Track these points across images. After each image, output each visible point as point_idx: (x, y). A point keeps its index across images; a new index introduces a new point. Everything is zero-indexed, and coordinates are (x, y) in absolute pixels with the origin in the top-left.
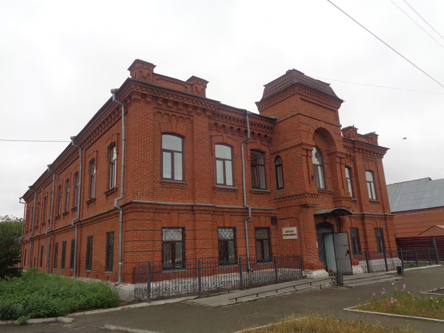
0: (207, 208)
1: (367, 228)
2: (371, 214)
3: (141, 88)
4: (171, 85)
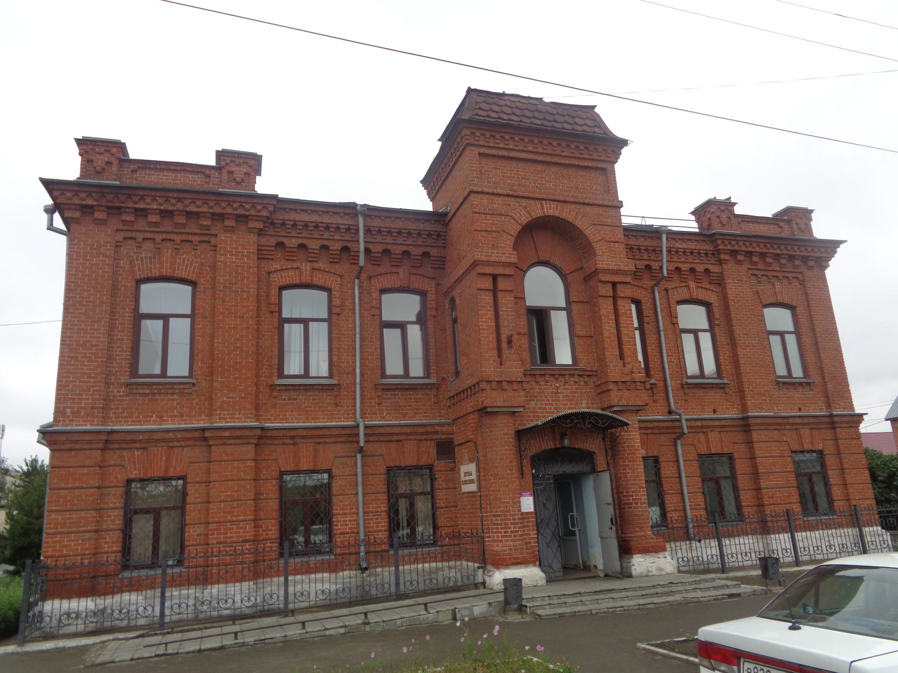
0: (238, 433)
1: (758, 453)
2: (776, 415)
3: (241, 206)
4: (171, 176)
